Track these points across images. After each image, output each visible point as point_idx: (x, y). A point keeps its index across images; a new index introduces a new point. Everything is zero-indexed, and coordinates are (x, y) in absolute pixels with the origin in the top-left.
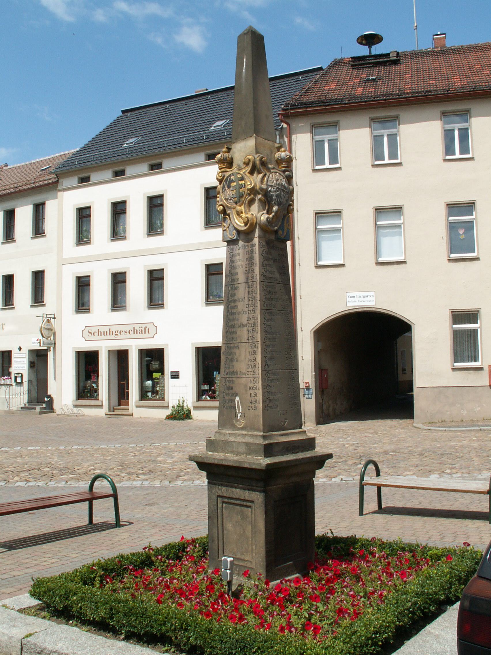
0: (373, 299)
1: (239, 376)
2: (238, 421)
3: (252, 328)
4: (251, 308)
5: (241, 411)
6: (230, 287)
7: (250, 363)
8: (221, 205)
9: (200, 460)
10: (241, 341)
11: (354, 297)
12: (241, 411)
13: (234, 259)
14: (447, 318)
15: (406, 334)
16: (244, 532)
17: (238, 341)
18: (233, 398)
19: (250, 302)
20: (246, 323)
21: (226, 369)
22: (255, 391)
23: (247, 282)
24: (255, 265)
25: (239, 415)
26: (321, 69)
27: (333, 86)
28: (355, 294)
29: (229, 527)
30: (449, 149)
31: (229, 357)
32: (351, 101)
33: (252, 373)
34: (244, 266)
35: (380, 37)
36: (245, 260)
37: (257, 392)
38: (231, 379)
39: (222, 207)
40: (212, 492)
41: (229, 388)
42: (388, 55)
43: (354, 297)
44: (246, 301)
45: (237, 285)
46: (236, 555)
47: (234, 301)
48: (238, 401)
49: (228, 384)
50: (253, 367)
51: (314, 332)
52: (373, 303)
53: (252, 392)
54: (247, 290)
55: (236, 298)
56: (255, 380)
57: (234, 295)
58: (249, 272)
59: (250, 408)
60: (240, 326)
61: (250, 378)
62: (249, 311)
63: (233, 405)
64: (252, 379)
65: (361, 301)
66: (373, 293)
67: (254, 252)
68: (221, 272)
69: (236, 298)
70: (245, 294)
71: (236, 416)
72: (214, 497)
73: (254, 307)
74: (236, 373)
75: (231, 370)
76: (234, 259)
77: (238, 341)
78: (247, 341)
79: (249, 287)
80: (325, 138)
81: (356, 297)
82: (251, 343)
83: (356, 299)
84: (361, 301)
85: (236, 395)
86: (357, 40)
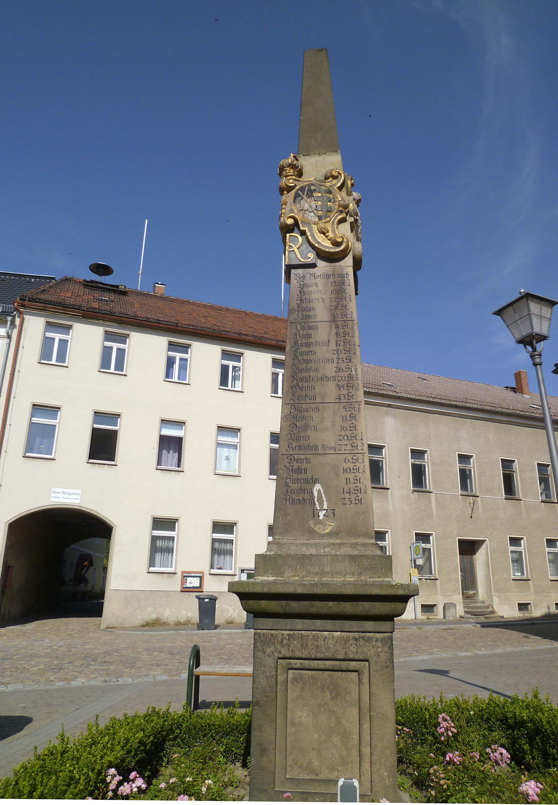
0: (79, 497)
1: (320, 452)
2: (318, 522)
3: (345, 383)
4: (342, 356)
5: (325, 507)
6: (298, 326)
7: (343, 433)
8: (291, 217)
9: (240, 590)
10: (323, 399)
11: (59, 493)
12: (325, 507)
13: (306, 289)
14: (149, 523)
15: (97, 540)
16: (338, 723)
17: (318, 400)
18: (308, 486)
19: (341, 348)
20: (333, 375)
21: (291, 441)
22: (356, 474)
23: (334, 320)
24: (348, 300)
25: (322, 514)
26: (54, 278)
27: (68, 294)
28: (60, 490)
29: (300, 717)
30: (168, 374)
31: (298, 423)
32: (89, 310)
33: (349, 447)
34: (327, 301)
35: (111, 270)
36: (329, 292)
37: (359, 475)
38: (303, 457)
39: (292, 221)
40: (265, 653)
41: (299, 471)
42: (117, 287)
43: (59, 493)
44: (333, 345)
45: (314, 324)
46: (317, 775)
47: (309, 345)
48: (319, 491)
49: (296, 465)
50: (350, 438)
51: (9, 524)
52: (78, 501)
53: (351, 476)
54: (334, 331)
55: (312, 340)
56: (354, 458)
57: (309, 336)
58: (336, 308)
59: (347, 501)
60: (322, 379)
61: (345, 456)
62: (338, 358)
63: (307, 496)
64: (349, 457)
65: (65, 498)
66: (79, 492)
67: (347, 284)
68: (170, 347)
69: (312, 340)
70: (329, 335)
71: (315, 515)
72: (270, 662)
73: (348, 354)
74: (316, 447)
75: (306, 443)
76: (306, 289)
77: (318, 400)
78: (337, 401)
79: (337, 327)
80: (56, 336)
81: (61, 493)
82: (345, 404)
83: (61, 495)
84: (65, 498)
85: (315, 481)
86: (90, 267)
